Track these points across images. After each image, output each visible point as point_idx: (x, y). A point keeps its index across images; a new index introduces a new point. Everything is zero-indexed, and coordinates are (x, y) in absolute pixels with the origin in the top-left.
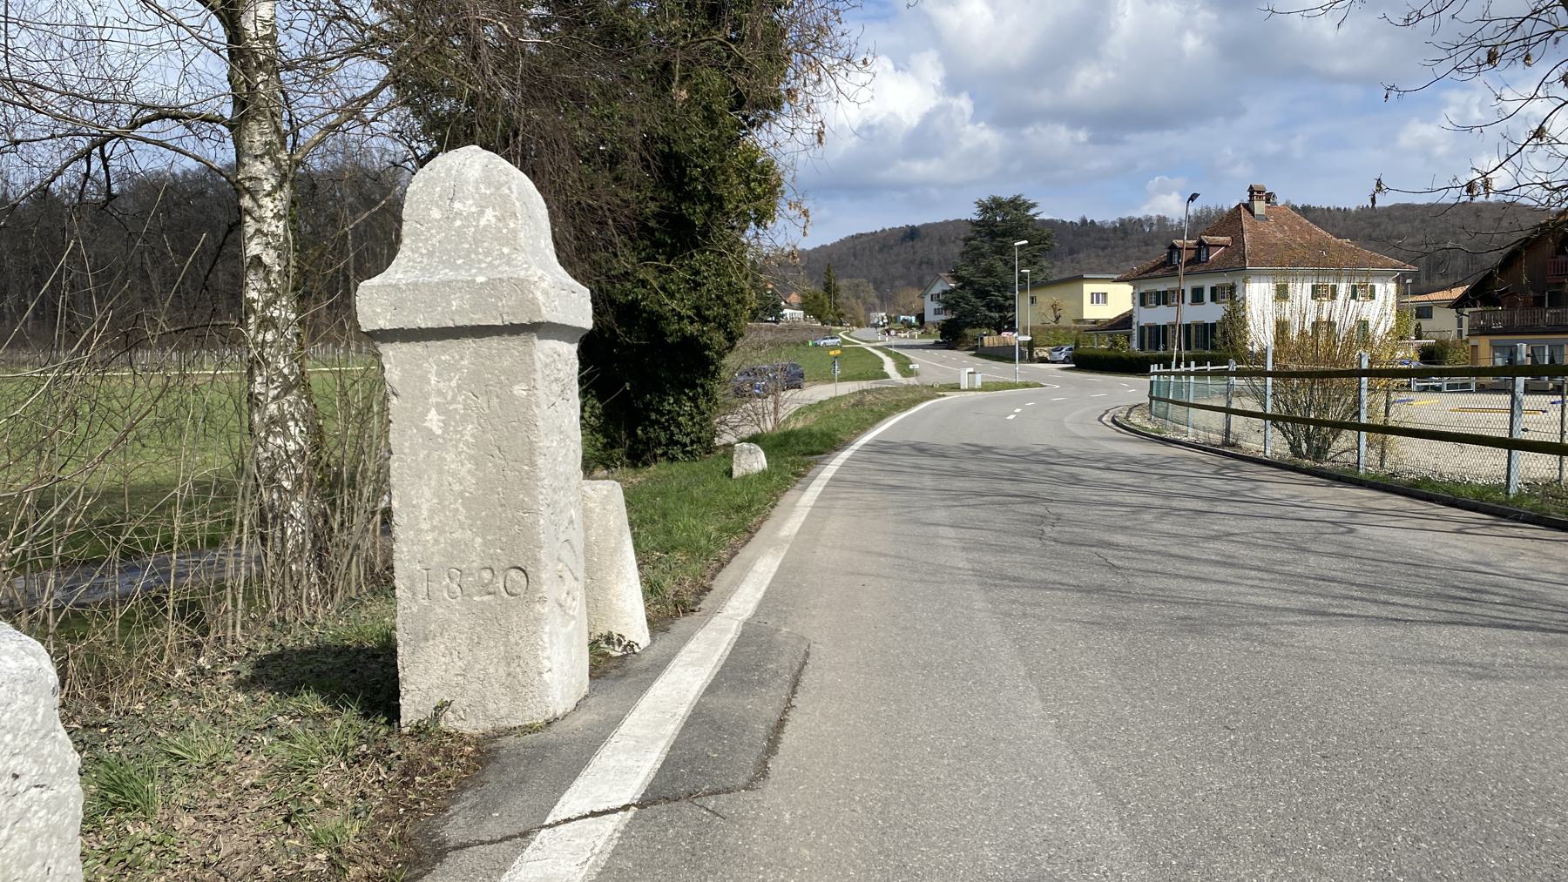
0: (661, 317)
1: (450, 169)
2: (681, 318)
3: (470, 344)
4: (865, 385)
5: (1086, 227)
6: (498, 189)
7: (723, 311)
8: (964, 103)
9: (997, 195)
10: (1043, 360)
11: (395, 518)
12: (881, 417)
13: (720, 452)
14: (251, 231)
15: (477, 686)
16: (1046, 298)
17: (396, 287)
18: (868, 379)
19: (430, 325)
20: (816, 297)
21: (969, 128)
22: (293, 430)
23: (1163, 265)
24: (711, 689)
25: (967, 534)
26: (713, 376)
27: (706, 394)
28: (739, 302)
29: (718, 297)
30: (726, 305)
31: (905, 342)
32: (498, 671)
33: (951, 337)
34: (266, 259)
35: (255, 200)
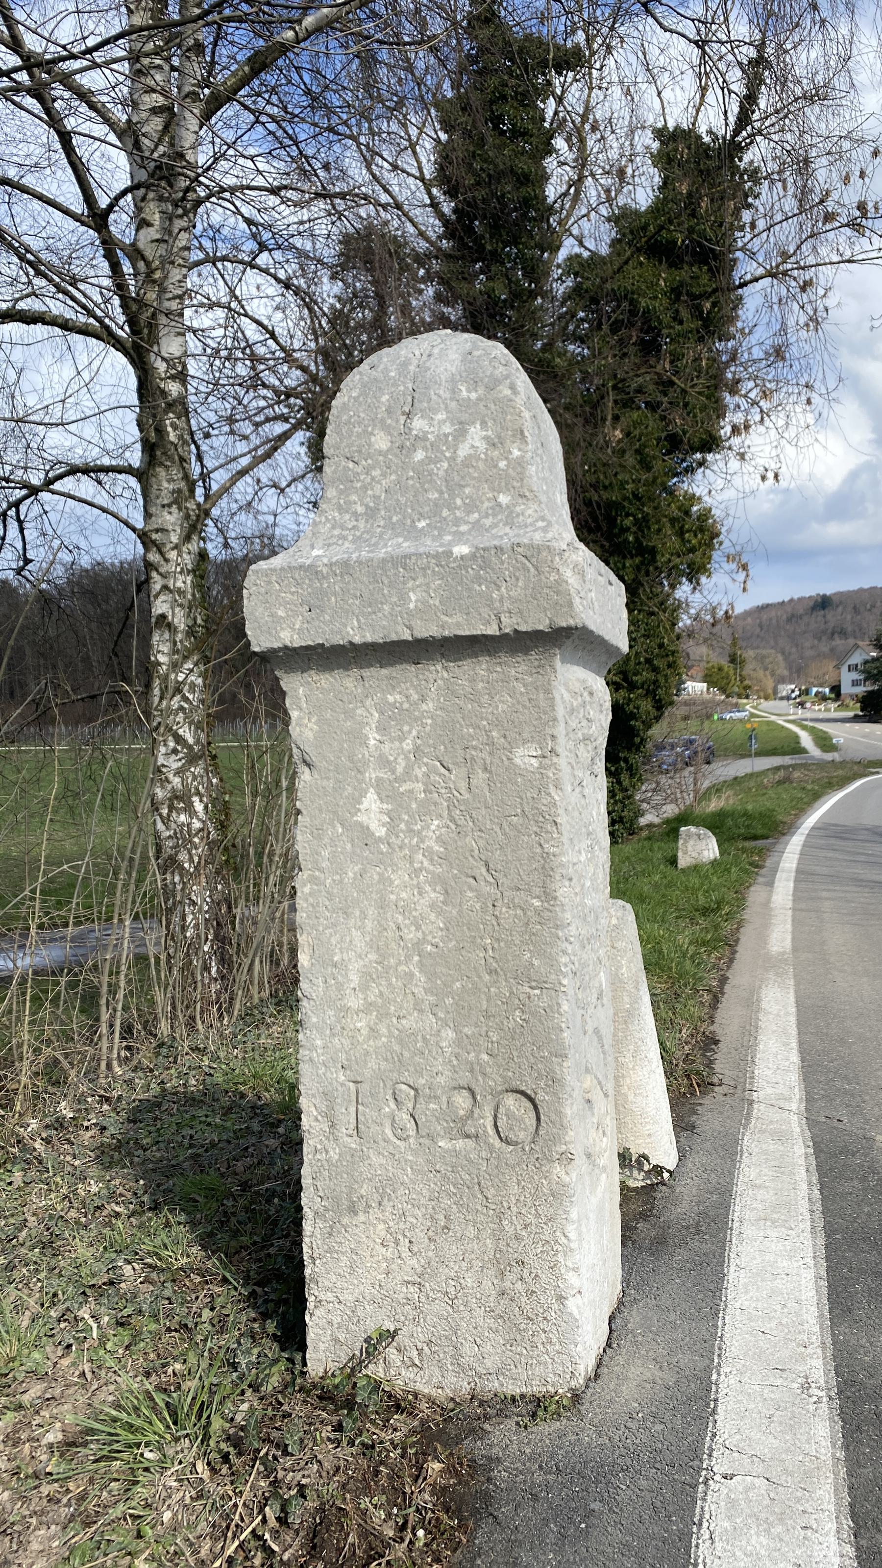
1: (405, 364)
3: (438, 673)
4: (787, 760)
6: (490, 389)
7: (652, 676)
11: (304, 984)
13: (644, 834)
14: (157, 587)
15: (441, 1307)
17: (311, 570)
18: (784, 754)
19: (369, 638)
20: (720, 669)
22: (199, 807)
26: (638, 749)
27: (630, 768)
28: (669, 666)
29: (648, 661)
31: (821, 716)
35: (162, 554)
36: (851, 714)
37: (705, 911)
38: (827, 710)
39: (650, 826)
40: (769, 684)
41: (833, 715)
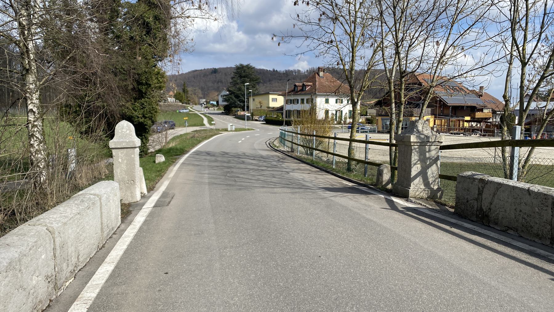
0: (132, 117)
2: (138, 117)
3: (125, 150)
4: (198, 128)
5: (275, 72)
7: (151, 115)
8: (234, 24)
9: (242, 63)
10: (256, 120)
12: (200, 142)
13: (150, 155)
14: (30, 102)
16: (258, 99)
20: (180, 94)
21: (236, 33)
23: (292, 91)
24: (160, 198)
25: (210, 176)
27: (145, 138)
30: (151, 113)
31: (212, 112)
32: (129, 195)
33: (228, 111)
34: (34, 110)
36: (221, 112)
37: (159, 171)
38: (214, 110)
39: (152, 152)
40: (196, 100)
41: (216, 112)
